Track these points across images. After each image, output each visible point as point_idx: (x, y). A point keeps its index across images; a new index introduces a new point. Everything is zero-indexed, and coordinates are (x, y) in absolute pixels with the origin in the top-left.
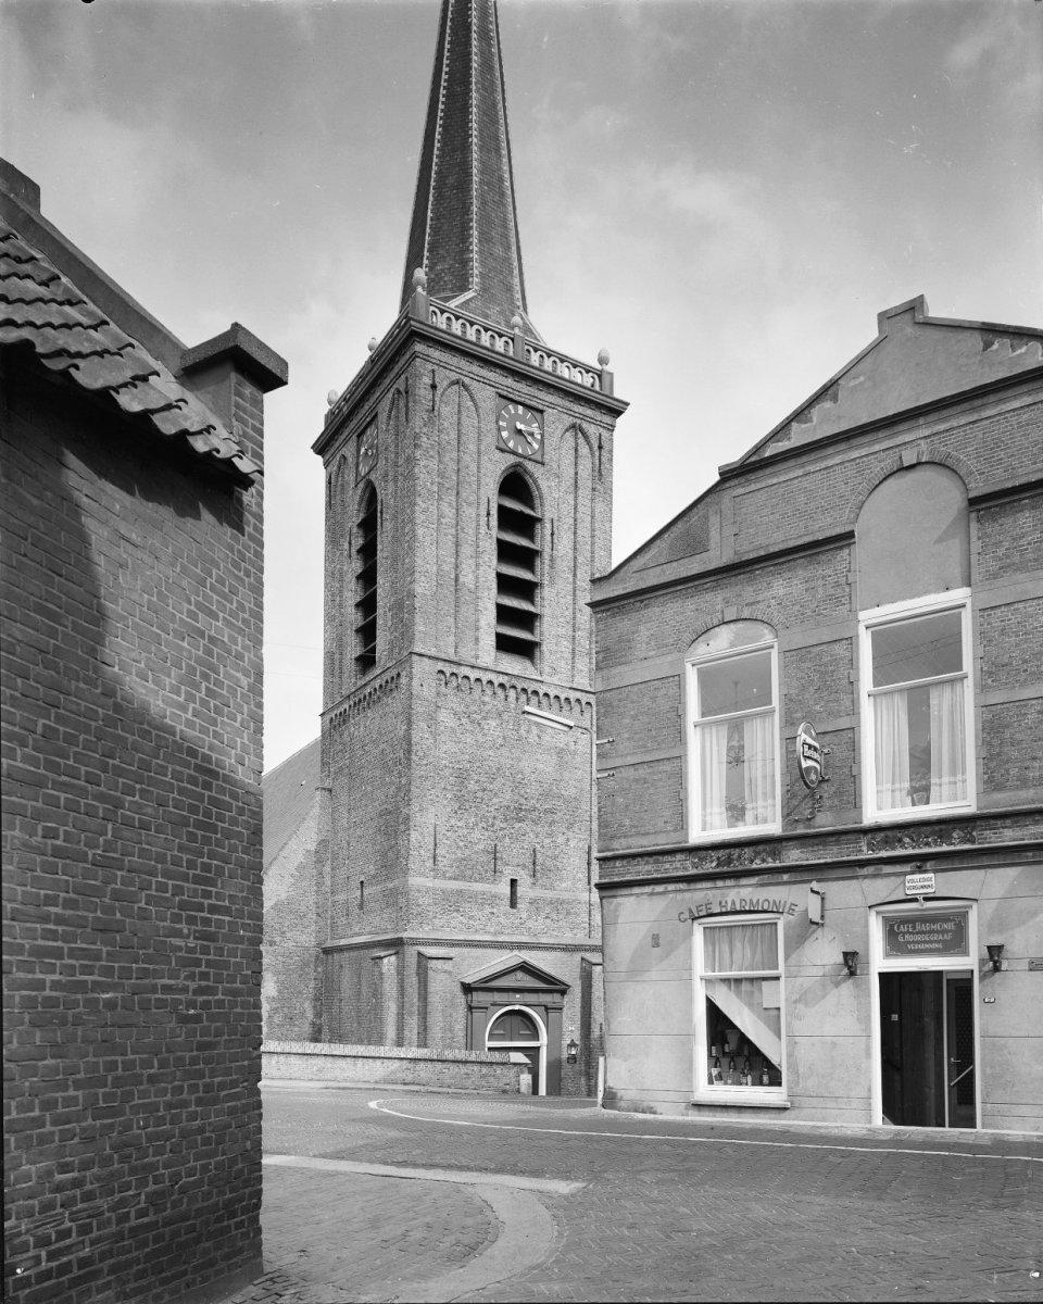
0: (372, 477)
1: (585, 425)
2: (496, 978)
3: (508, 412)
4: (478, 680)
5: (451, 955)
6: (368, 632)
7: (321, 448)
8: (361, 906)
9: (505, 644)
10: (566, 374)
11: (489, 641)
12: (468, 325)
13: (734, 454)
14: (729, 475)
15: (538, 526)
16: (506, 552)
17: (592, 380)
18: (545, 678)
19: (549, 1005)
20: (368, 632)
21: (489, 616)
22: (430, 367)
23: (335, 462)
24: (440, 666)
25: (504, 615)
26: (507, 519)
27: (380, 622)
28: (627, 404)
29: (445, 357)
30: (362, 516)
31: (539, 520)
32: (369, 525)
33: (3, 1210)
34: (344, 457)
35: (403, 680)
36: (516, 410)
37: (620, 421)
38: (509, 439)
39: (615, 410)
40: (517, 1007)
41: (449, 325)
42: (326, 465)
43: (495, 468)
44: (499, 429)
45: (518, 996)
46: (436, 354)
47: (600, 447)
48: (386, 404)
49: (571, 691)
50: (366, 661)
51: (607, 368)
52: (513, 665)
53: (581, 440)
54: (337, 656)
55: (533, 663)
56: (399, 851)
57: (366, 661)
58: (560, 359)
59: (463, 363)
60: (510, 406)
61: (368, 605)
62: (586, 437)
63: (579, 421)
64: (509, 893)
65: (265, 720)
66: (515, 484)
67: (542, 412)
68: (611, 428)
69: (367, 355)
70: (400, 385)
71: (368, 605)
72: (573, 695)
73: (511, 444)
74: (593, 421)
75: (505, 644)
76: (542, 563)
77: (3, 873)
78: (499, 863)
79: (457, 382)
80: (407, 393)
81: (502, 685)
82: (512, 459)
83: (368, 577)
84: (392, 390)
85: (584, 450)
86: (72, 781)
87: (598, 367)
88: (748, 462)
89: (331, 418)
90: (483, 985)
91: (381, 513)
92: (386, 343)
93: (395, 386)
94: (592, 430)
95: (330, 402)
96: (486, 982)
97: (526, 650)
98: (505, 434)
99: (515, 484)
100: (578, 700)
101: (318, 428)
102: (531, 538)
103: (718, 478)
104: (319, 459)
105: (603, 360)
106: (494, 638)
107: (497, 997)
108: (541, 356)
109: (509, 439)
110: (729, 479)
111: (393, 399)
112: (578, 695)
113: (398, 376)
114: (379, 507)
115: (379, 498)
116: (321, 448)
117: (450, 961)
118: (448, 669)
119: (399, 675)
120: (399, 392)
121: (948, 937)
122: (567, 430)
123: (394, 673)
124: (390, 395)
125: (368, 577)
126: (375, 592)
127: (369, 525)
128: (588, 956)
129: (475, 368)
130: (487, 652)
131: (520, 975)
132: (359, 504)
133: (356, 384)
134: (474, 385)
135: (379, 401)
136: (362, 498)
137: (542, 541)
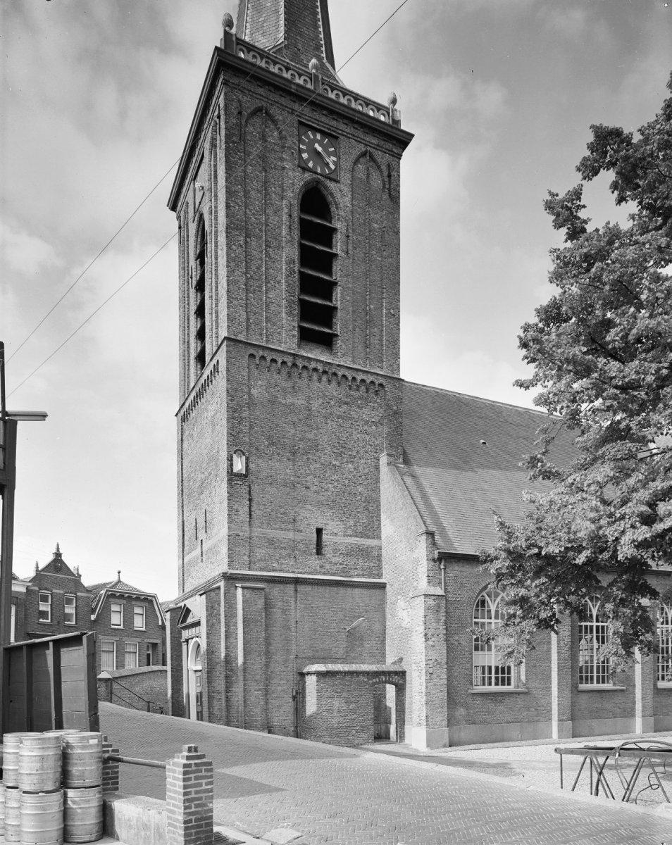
2: (15, 415)
3: (308, 137)
9: (306, 336)
10: (353, 105)
12: (329, 89)
28: (412, 136)
36: (315, 136)
38: (308, 160)
43: (295, 181)
44: (300, 151)
52: (317, 354)
56: (620, 277)
60: (309, 133)
64: (315, 539)
67: (337, 138)
73: (311, 165)
74: (377, 147)
75: (306, 336)
76: (337, 294)
79: (259, 110)
81: (315, 370)
82: (308, 176)
86: (331, 667)
94: (378, 155)
98: (305, 156)
102: (331, 328)
109: (308, 160)
117: (244, 844)
122: (356, 162)
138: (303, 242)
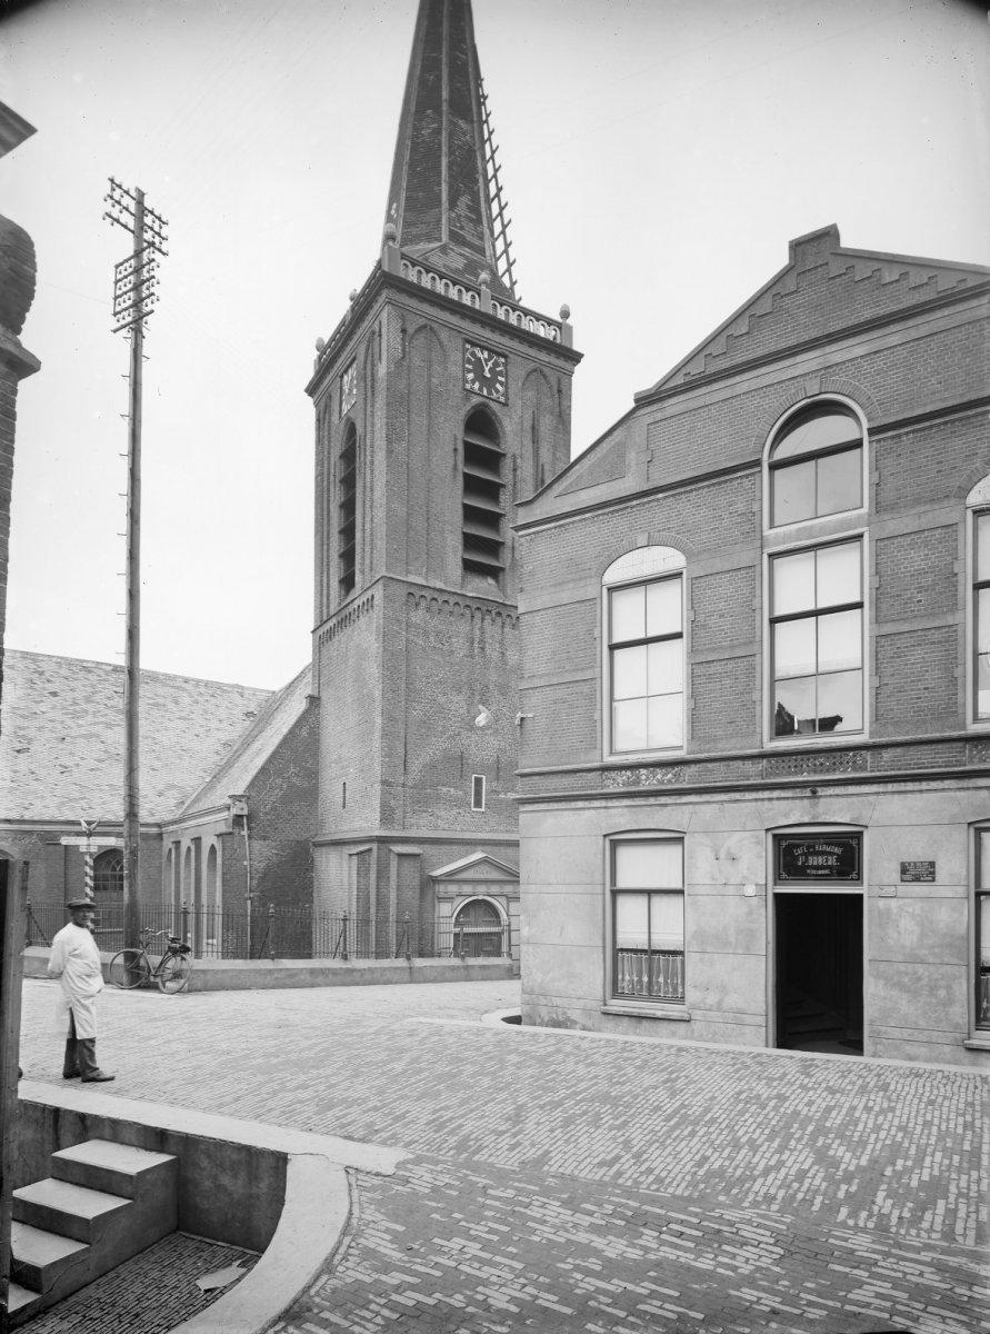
4: (478, 609)
7: (312, 390)
9: (470, 567)
13: (648, 382)
14: (644, 401)
15: (501, 575)
16: (472, 485)
17: (554, 332)
31: (504, 455)
33: (526, 1314)
37: (578, 369)
39: (576, 358)
40: (481, 898)
41: (419, 278)
50: (348, 582)
51: (569, 321)
52: (482, 587)
55: (497, 581)
57: (348, 582)
58: (466, 288)
61: (348, 532)
62: (545, 377)
65: (14, 476)
66: (481, 422)
69: (348, 304)
71: (348, 532)
75: (470, 567)
77: (7, 660)
78: (465, 767)
87: (560, 320)
88: (666, 387)
97: (494, 572)
99: (481, 422)
101: (309, 374)
103: (633, 405)
107: (467, 889)
108: (507, 310)
110: (644, 406)
121: (832, 861)
131: (485, 868)
137: (506, 477)
138: (467, 557)
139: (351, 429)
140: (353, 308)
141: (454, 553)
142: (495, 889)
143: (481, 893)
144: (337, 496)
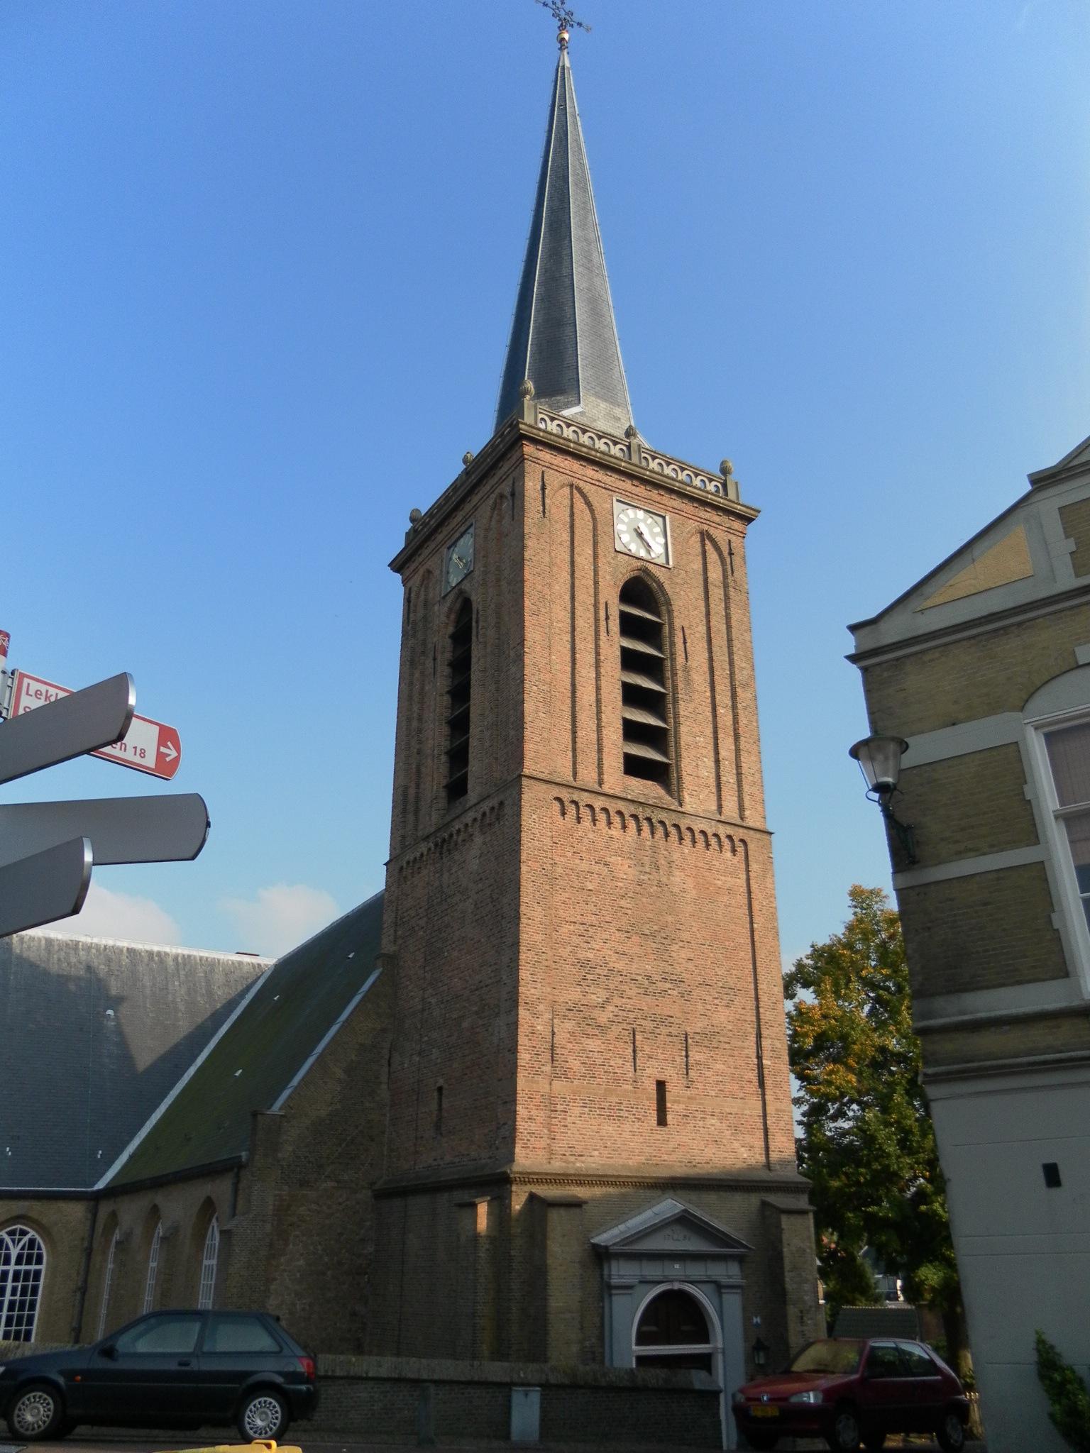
0: (466, 586)
1: (712, 531)
5: (612, 633)
6: (458, 757)
7: (399, 565)
8: (438, 1127)
9: (634, 767)
11: (614, 763)
18: (687, 808)
19: (724, 1281)
20: (458, 757)
21: (614, 733)
22: (539, 469)
23: (417, 579)
24: (557, 791)
25: (632, 731)
26: (630, 626)
27: (473, 743)
29: (559, 460)
30: (451, 629)
32: (462, 637)
34: (429, 572)
35: (508, 810)
36: (628, 516)
40: (676, 1286)
42: (404, 582)
45: (677, 1266)
46: (546, 456)
47: (731, 554)
48: (485, 510)
49: (720, 825)
50: (457, 789)
52: (641, 788)
53: (709, 546)
54: (412, 791)
57: (457, 789)
59: (575, 465)
61: (459, 725)
63: (706, 527)
68: (743, 535)
70: (506, 488)
71: (459, 725)
72: (723, 831)
80: (513, 494)
83: (460, 693)
84: (493, 496)
85: (713, 556)
89: (411, 536)
90: (627, 1249)
91: (477, 622)
92: (483, 455)
93: (497, 491)
94: (718, 534)
95: (412, 520)
96: (631, 1243)
100: (730, 837)
101: (397, 545)
104: (398, 577)
105: (725, 471)
106: (618, 653)
107: (652, 1270)
111: (495, 503)
112: (730, 830)
113: (502, 481)
114: (474, 616)
115: (474, 606)
116: (399, 565)
118: (565, 795)
119: (501, 804)
120: (502, 496)
123: (494, 802)
124: (491, 502)
125: (460, 693)
126: (467, 743)
127: (462, 637)
128: (772, 1198)
129: (590, 472)
130: (616, 779)
132: (448, 617)
133: (438, 506)
134: (587, 488)
135: (476, 508)
136: (450, 609)
138: (628, 716)
139: (465, 606)
140: (467, 473)
141: (616, 746)
142: (697, 1270)
143: (677, 1276)
144: (440, 684)
